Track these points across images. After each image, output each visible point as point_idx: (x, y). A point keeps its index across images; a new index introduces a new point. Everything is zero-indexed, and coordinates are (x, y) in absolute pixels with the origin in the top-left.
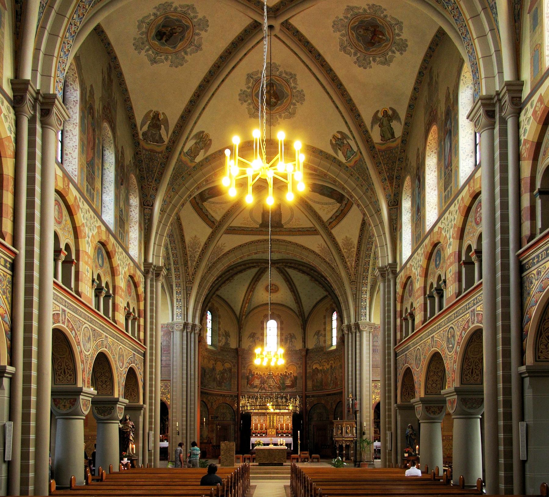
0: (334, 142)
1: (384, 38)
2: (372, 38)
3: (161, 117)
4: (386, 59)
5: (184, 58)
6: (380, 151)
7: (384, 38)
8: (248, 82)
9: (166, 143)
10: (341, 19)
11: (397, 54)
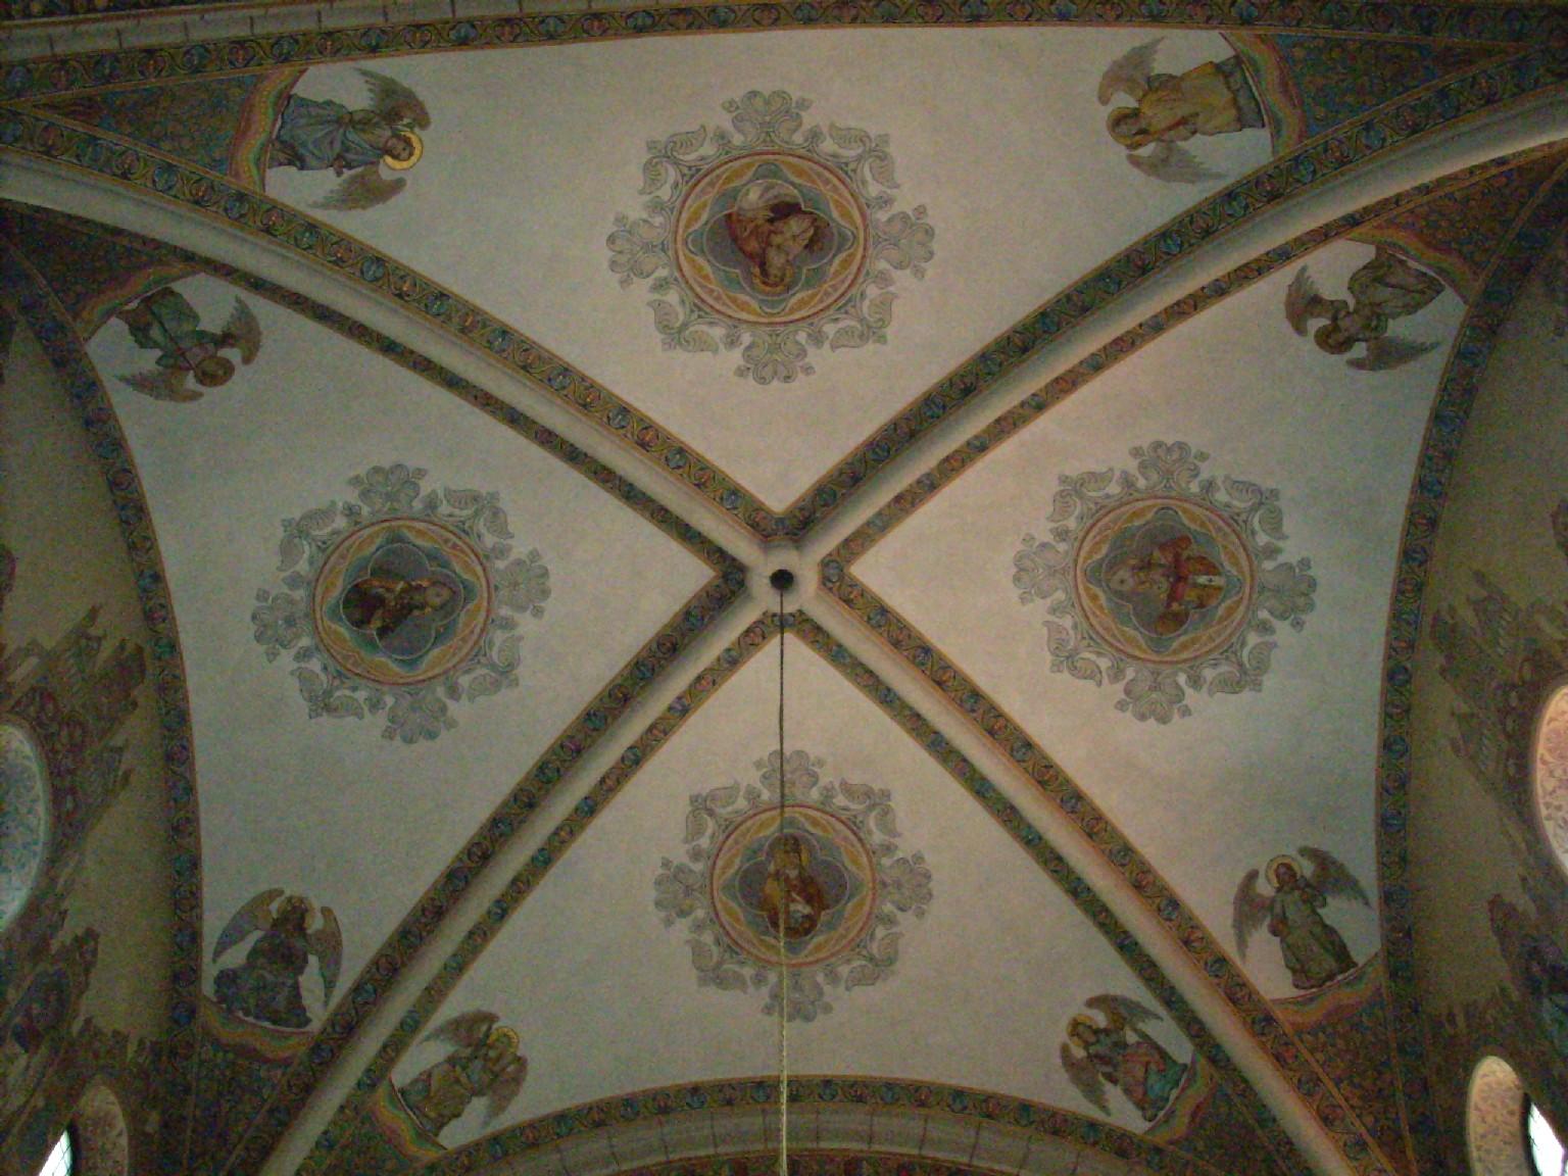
0: (1079, 1053)
1: (1218, 581)
2: (1173, 596)
3: (315, 924)
4: (1241, 665)
5: (444, 709)
6: (1300, 1031)
7: (1218, 581)
8: (695, 830)
9: (315, 1026)
10: (1044, 545)
11: (1283, 630)
